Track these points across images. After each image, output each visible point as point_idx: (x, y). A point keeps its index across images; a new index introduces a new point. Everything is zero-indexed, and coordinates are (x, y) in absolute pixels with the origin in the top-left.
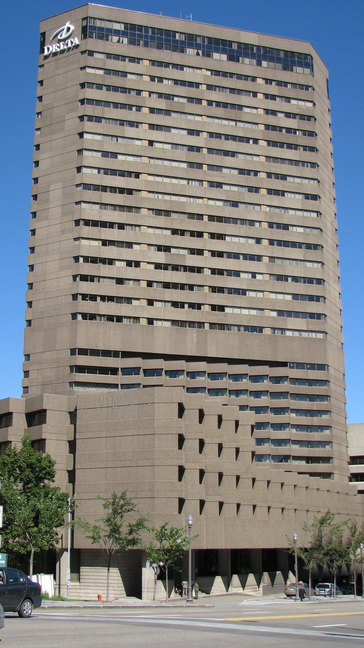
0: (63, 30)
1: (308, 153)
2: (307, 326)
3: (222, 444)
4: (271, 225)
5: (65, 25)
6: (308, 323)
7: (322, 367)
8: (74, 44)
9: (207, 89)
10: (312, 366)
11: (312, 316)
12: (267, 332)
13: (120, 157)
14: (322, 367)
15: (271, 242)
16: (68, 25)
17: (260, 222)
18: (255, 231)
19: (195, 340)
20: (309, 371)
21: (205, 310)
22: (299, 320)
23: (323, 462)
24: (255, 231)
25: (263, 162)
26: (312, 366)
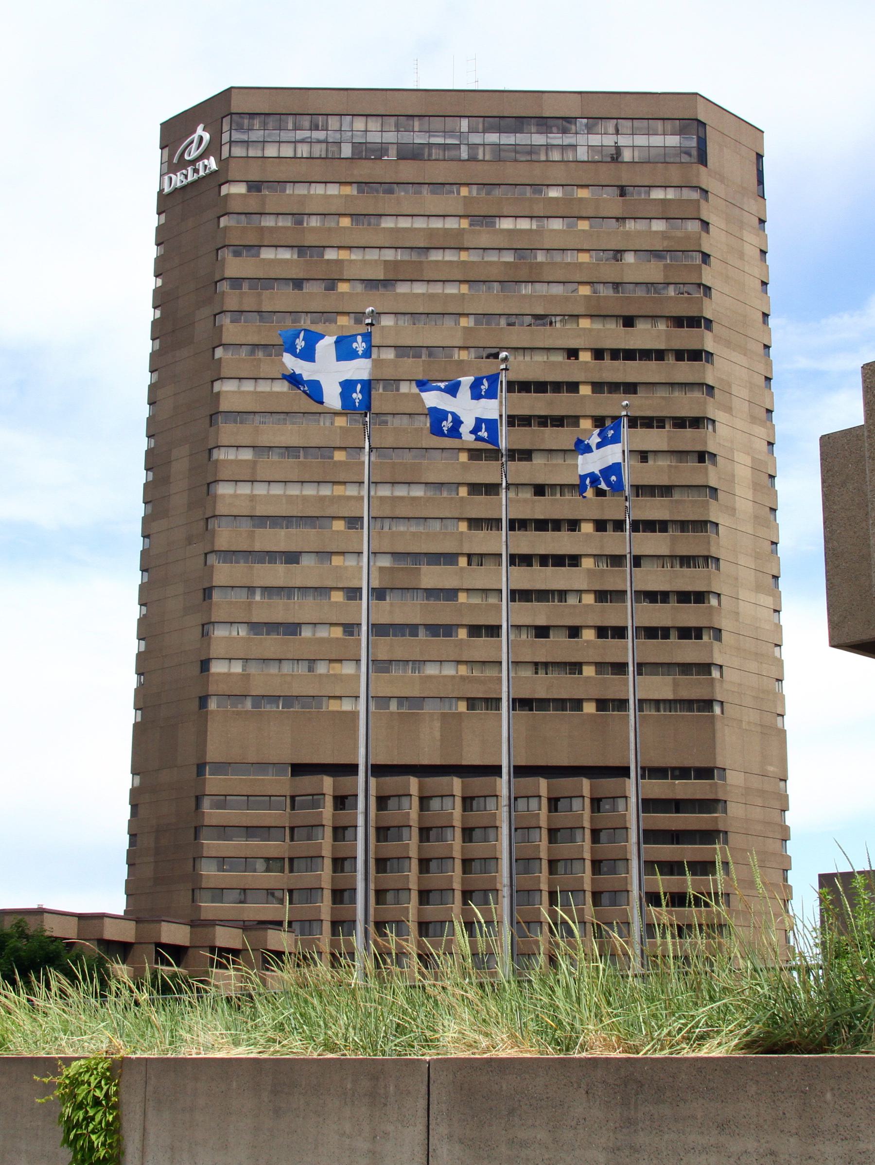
0: (192, 142)
1: (685, 365)
2: (675, 691)
3: (472, 399)
4: (598, 354)
5: (195, 132)
6: (676, 685)
7: (706, 773)
10: (683, 773)
11: (686, 668)
12: (589, 708)
13: (306, 633)
14: (706, 773)
15: (598, 387)
16: (200, 130)
17: (580, 592)
18: (564, 335)
19: (437, 734)
20: (677, 782)
21: (460, 673)
22: (657, 679)
23: (698, 674)
24: (564, 335)
25: (587, 362)
26: (683, 773)
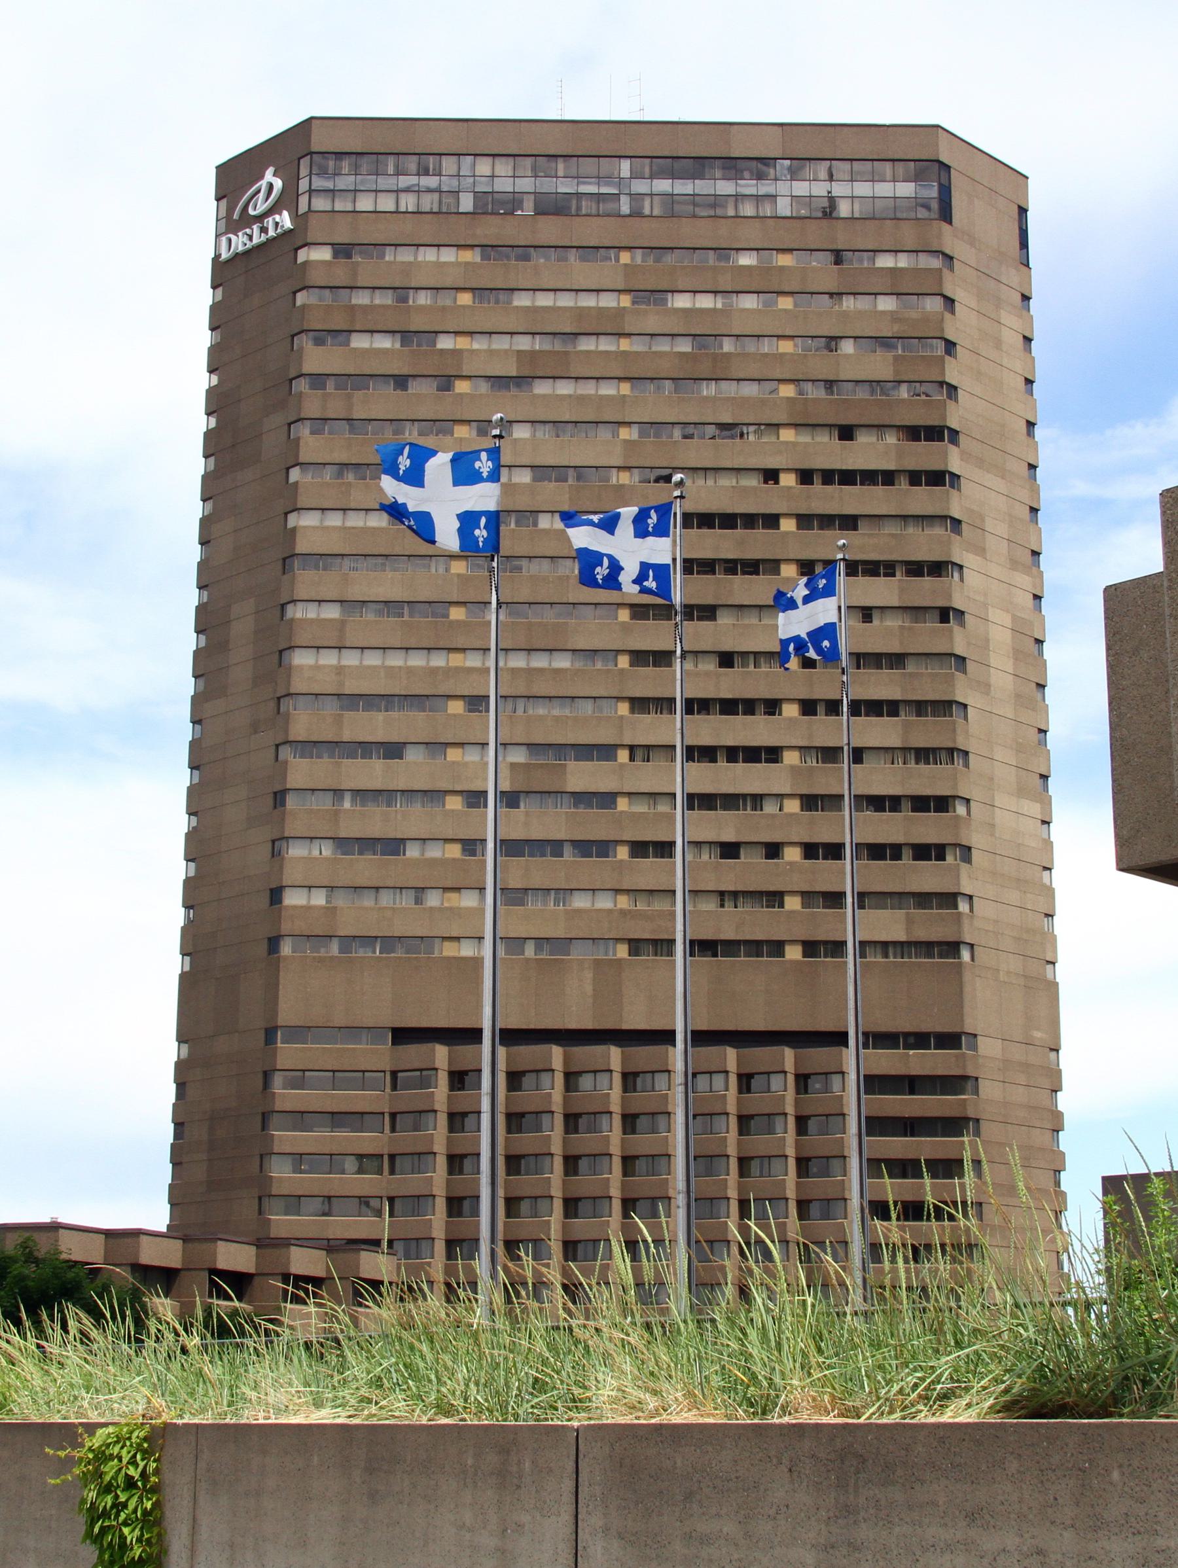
0: (259, 191)
1: (922, 491)
2: (908, 930)
3: (636, 536)
4: (805, 477)
5: (262, 177)
6: (910, 921)
7: (950, 1040)
8: (279, 230)
9: (632, 711)
10: (920, 1040)
11: (923, 899)
12: (794, 953)
13: (413, 851)
14: (950, 1040)
15: (805, 520)
16: (269, 175)
17: (781, 796)
18: (759, 451)
19: (589, 989)
20: (911, 1052)
21: (619, 906)
22: (885, 914)
23: (940, 907)
24: (759, 451)
25: (790, 488)
26: (920, 1040)
